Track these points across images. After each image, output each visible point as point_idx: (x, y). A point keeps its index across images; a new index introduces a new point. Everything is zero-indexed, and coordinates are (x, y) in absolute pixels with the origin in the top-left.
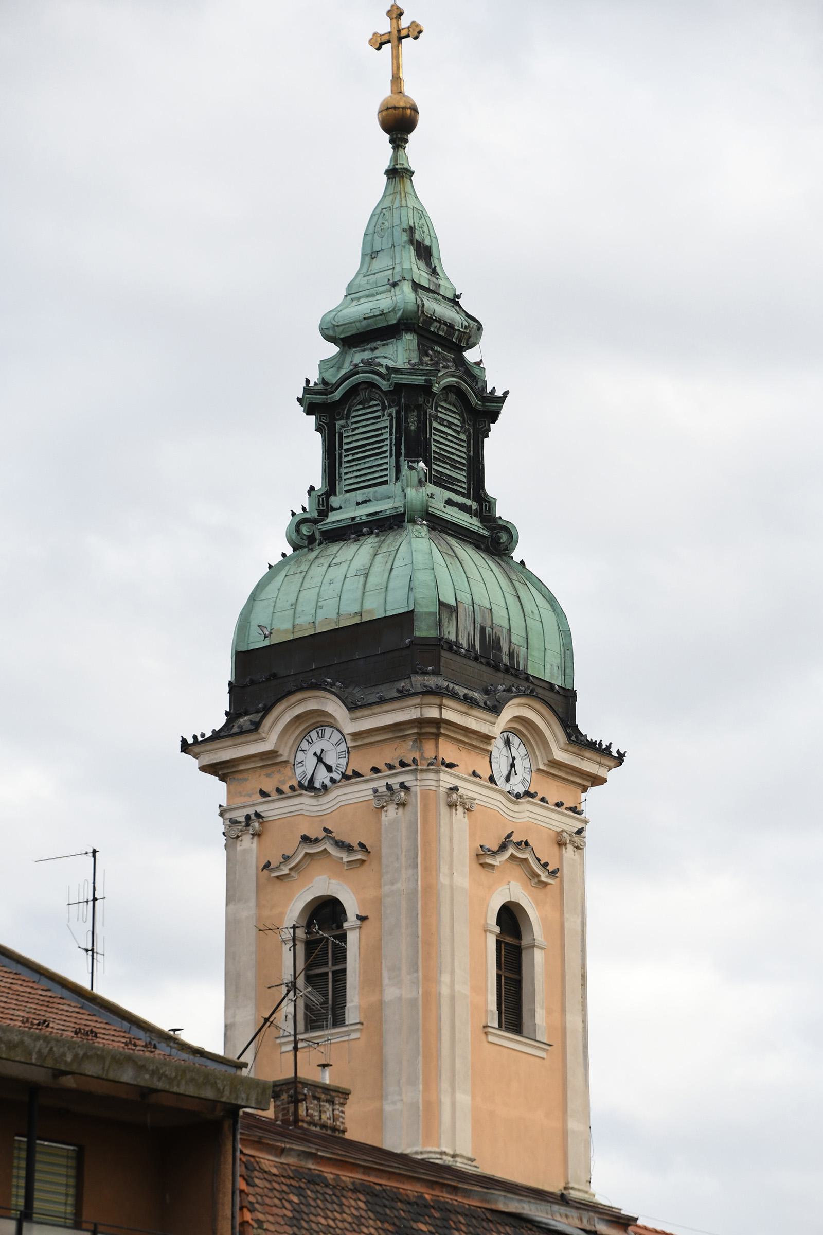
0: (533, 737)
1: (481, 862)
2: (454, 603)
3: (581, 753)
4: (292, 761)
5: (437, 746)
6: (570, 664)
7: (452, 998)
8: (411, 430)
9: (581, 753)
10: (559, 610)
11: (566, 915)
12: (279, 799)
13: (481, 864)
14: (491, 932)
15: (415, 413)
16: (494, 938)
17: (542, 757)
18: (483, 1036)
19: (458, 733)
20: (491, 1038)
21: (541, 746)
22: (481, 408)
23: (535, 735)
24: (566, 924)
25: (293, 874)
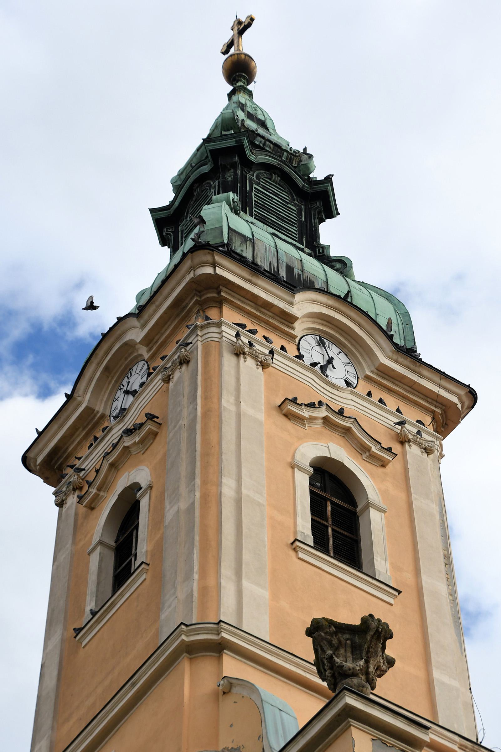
0: (356, 348)
1: (284, 412)
2: (251, 237)
3: (417, 369)
4: (108, 413)
5: (221, 312)
6: (410, 333)
7: (239, 502)
8: (228, 182)
9: (417, 369)
10: (396, 302)
11: (414, 495)
12: (98, 444)
13: (286, 415)
14: (301, 469)
15: (232, 171)
16: (307, 477)
17: (369, 366)
18: (292, 553)
19: (247, 304)
20: (301, 555)
21: (365, 356)
22: (309, 191)
23: (358, 346)
24: (414, 502)
25: (101, 493)
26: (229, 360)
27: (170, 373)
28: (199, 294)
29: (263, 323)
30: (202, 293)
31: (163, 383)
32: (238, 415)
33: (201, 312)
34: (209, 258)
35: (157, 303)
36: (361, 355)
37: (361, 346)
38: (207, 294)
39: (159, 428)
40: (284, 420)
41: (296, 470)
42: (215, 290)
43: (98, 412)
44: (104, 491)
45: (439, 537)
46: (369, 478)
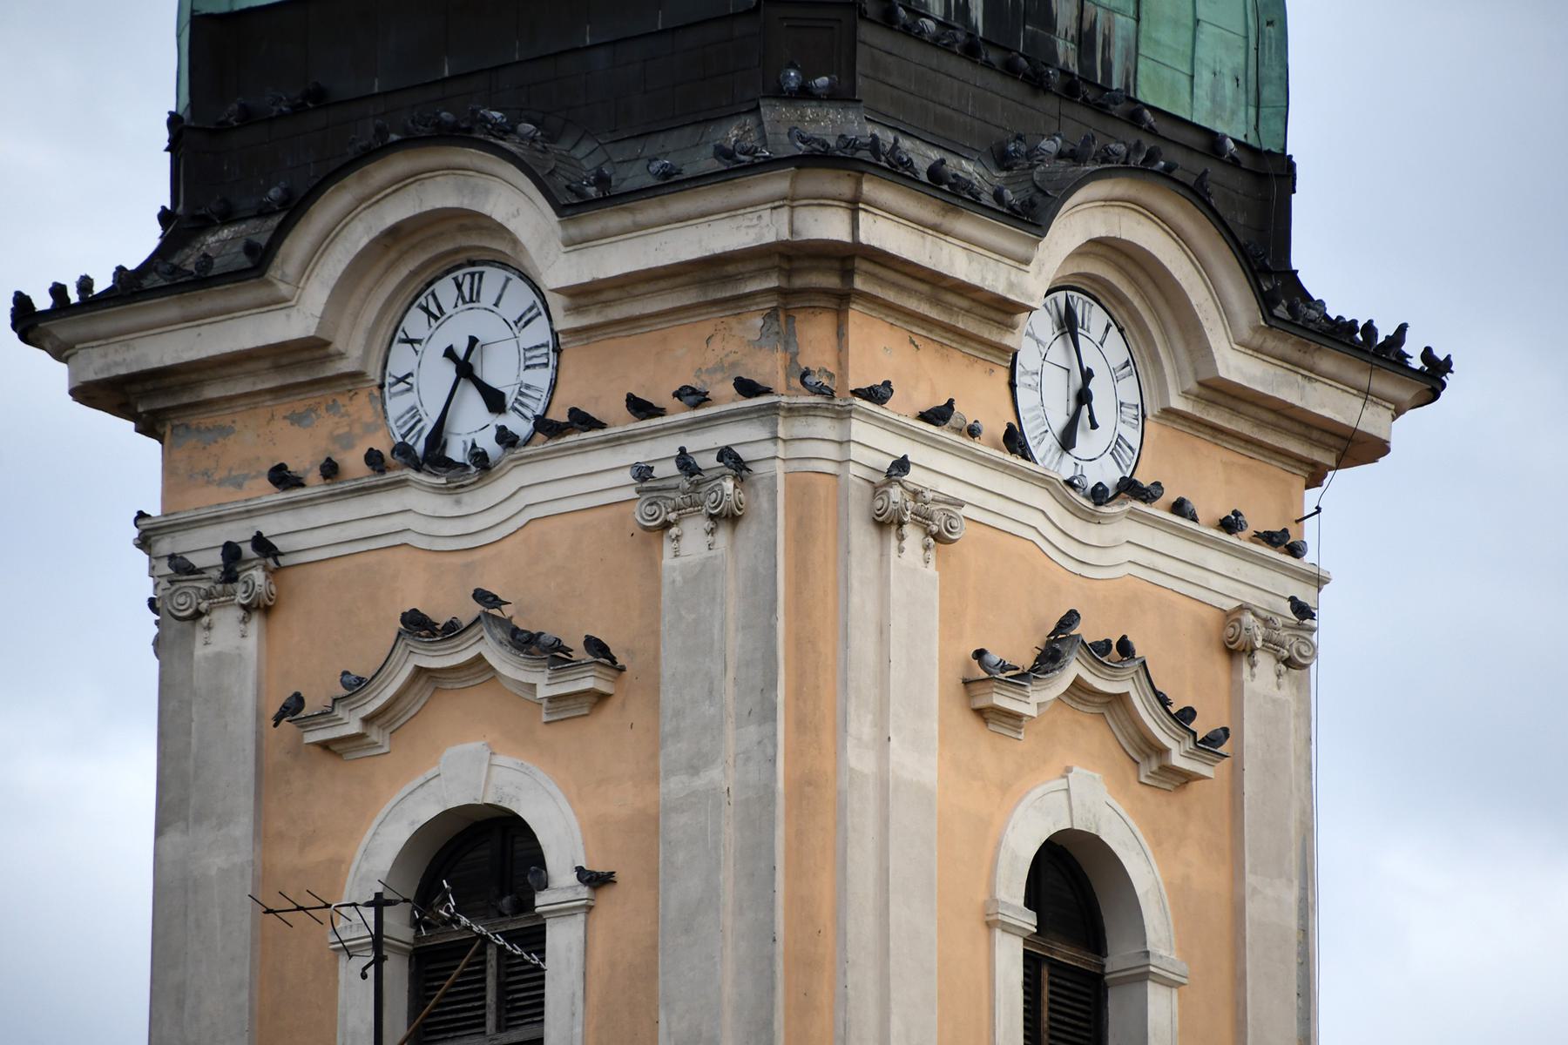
4: (374, 373)
5: (841, 333)
6: (1278, 70)
9: (1307, 359)
11: (1250, 879)
13: (980, 713)
25: (375, 735)
26: (861, 536)
27: (672, 516)
28: (786, 266)
29: (938, 331)
30: (796, 264)
31: (631, 493)
32: (883, 785)
33: (782, 317)
34: (845, 187)
35: (641, 217)
36: (1164, 331)
37: (1157, 286)
38: (811, 270)
39: (615, 680)
40: (974, 723)
41: (998, 933)
42: (837, 265)
43: (341, 355)
44: (383, 727)
45: (1294, 967)
46: (1152, 860)
